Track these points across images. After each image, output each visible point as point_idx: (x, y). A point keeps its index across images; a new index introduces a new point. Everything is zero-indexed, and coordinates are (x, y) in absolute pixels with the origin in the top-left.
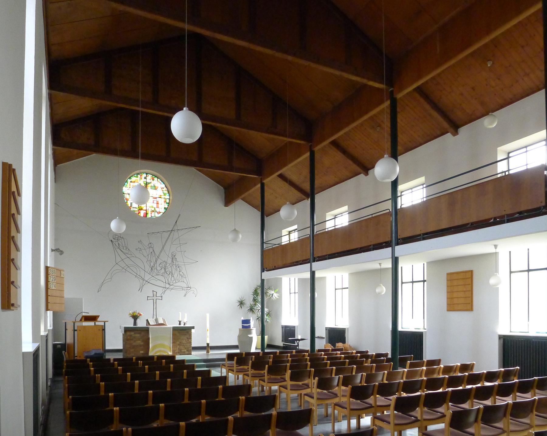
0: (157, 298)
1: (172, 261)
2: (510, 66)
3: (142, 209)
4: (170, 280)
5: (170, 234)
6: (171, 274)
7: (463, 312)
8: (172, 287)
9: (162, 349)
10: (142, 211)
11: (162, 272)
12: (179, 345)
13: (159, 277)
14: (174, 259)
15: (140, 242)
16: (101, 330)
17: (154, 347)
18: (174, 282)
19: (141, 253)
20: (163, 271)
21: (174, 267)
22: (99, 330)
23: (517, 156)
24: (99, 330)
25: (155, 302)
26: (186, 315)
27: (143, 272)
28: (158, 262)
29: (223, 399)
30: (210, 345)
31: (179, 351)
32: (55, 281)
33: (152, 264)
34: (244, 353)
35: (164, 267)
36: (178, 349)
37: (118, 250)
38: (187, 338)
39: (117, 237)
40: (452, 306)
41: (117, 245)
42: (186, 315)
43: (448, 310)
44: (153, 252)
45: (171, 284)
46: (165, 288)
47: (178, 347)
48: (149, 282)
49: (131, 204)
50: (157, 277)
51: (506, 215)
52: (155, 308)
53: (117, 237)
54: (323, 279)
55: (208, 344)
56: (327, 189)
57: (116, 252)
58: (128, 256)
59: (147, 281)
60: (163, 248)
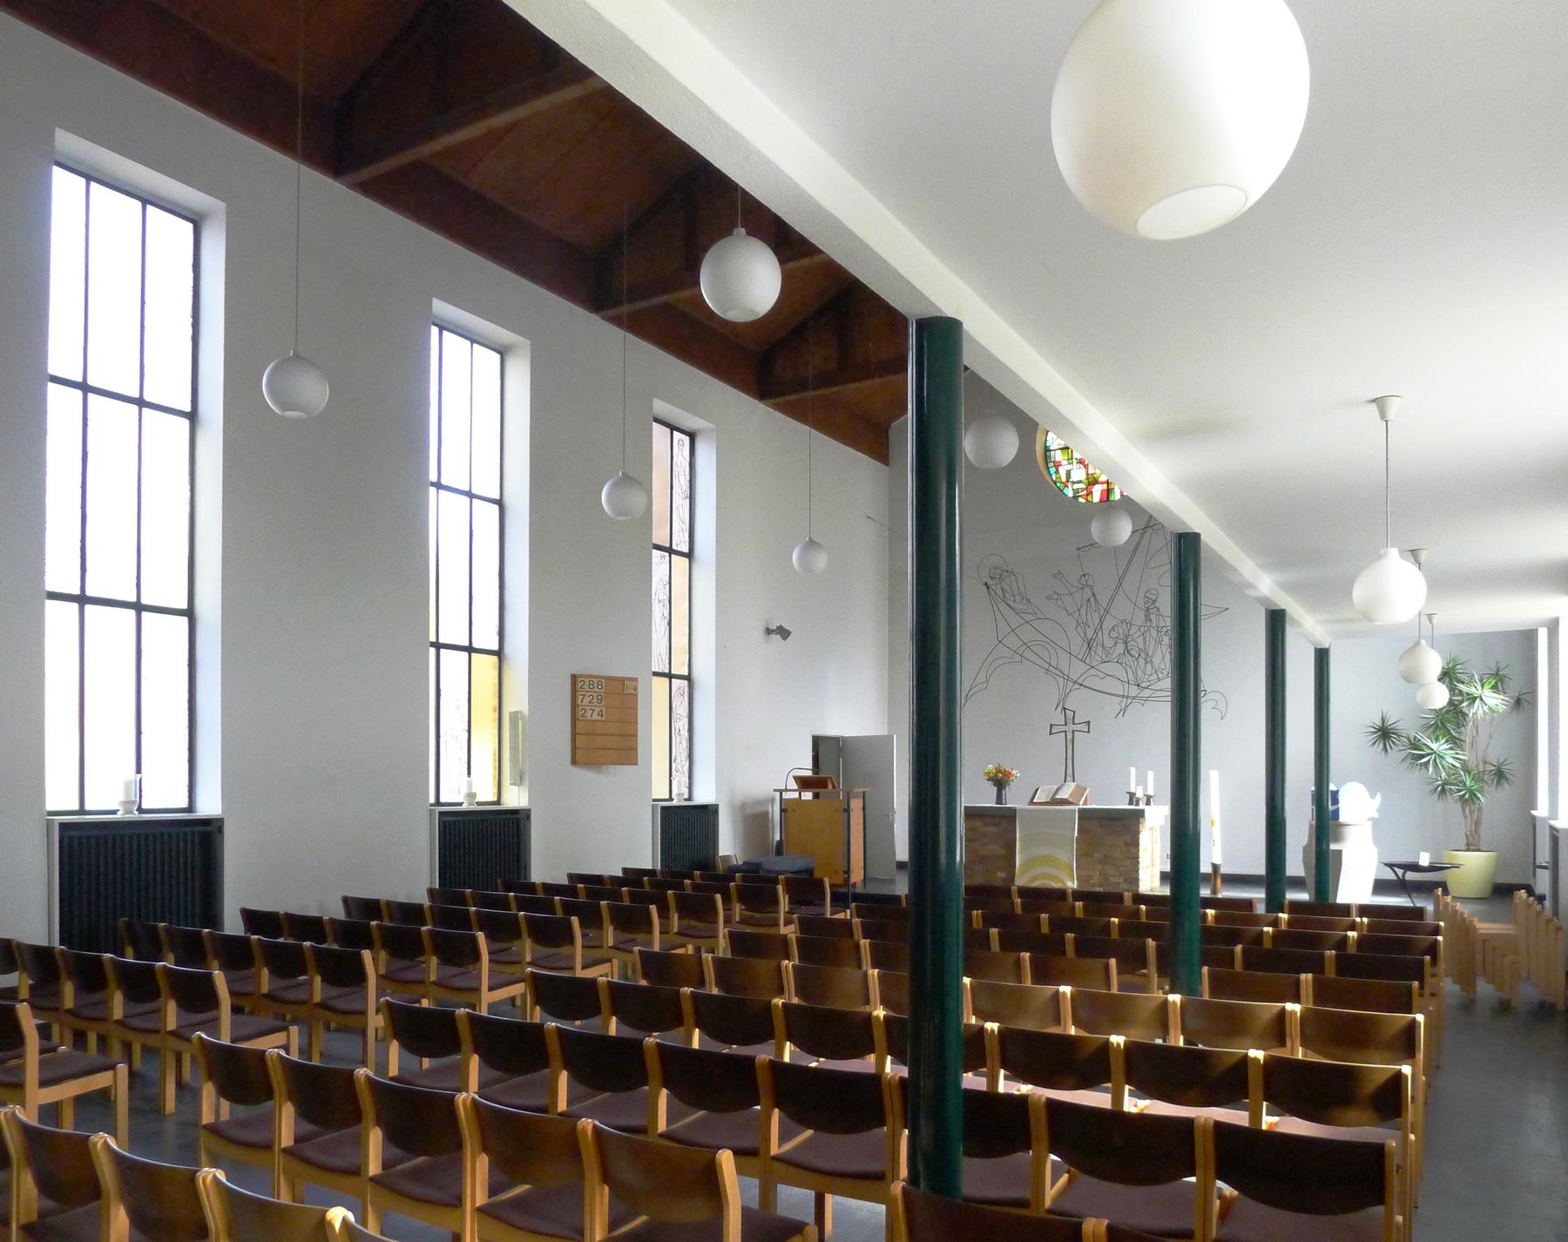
0: (1063, 728)
1: (1148, 619)
3: (1096, 482)
4: (1140, 673)
5: (1141, 538)
6: (1143, 655)
8: (1147, 693)
9: (1053, 871)
10: (1097, 486)
11: (1116, 653)
12: (1102, 862)
13: (1112, 668)
14: (1151, 611)
15: (1058, 575)
16: (841, 810)
17: (1028, 864)
18: (1155, 677)
19: (1061, 604)
20: (1120, 648)
21: (1154, 633)
25: (1069, 738)
26: (1151, 774)
27: (1064, 657)
28: (1107, 624)
29: (644, 983)
30: (1223, 870)
31: (1102, 881)
32: (603, 704)
33: (1090, 634)
35: (1122, 636)
36: (1098, 873)
37: (1002, 606)
38: (1127, 844)
39: (998, 571)
41: (999, 592)
42: (1151, 774)
44: (1092, 599)
45: (1143, 685)
46: (1128, 697)
47: (1099, 867)
48: (1081, 685)
49: (1068, 474)
50: (1103, 667)
52: (1070, 755)
53: (998, 571)
55: (1215, 867)
57: (996, 609)
58: (1028, 617)
59: (1075, 682)
60: (1120, 583)
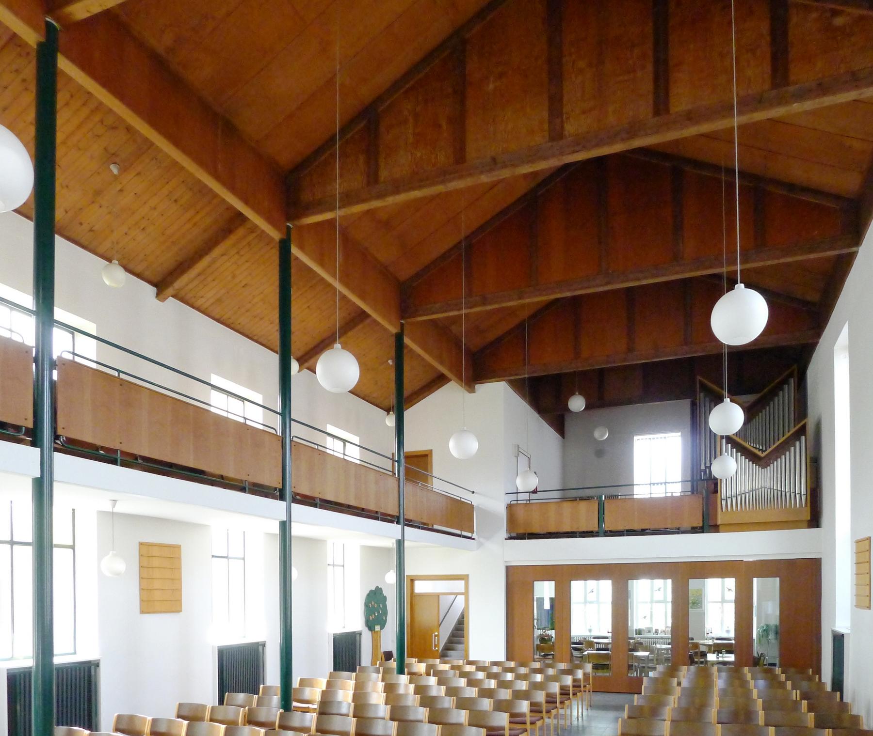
2: (238, 265)
7: (160, 614)
22: (590, 626)
23: (452, 485)
24: (728, 627)
34: (150, 718)
40: (148, 605)
43: (142, 612)
51: (24, 428)
54: (314, 543)
56: (230, 329)
